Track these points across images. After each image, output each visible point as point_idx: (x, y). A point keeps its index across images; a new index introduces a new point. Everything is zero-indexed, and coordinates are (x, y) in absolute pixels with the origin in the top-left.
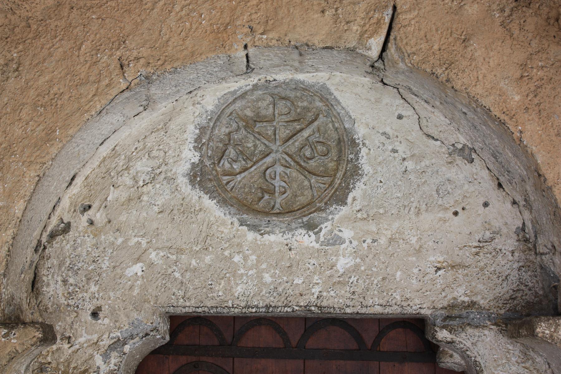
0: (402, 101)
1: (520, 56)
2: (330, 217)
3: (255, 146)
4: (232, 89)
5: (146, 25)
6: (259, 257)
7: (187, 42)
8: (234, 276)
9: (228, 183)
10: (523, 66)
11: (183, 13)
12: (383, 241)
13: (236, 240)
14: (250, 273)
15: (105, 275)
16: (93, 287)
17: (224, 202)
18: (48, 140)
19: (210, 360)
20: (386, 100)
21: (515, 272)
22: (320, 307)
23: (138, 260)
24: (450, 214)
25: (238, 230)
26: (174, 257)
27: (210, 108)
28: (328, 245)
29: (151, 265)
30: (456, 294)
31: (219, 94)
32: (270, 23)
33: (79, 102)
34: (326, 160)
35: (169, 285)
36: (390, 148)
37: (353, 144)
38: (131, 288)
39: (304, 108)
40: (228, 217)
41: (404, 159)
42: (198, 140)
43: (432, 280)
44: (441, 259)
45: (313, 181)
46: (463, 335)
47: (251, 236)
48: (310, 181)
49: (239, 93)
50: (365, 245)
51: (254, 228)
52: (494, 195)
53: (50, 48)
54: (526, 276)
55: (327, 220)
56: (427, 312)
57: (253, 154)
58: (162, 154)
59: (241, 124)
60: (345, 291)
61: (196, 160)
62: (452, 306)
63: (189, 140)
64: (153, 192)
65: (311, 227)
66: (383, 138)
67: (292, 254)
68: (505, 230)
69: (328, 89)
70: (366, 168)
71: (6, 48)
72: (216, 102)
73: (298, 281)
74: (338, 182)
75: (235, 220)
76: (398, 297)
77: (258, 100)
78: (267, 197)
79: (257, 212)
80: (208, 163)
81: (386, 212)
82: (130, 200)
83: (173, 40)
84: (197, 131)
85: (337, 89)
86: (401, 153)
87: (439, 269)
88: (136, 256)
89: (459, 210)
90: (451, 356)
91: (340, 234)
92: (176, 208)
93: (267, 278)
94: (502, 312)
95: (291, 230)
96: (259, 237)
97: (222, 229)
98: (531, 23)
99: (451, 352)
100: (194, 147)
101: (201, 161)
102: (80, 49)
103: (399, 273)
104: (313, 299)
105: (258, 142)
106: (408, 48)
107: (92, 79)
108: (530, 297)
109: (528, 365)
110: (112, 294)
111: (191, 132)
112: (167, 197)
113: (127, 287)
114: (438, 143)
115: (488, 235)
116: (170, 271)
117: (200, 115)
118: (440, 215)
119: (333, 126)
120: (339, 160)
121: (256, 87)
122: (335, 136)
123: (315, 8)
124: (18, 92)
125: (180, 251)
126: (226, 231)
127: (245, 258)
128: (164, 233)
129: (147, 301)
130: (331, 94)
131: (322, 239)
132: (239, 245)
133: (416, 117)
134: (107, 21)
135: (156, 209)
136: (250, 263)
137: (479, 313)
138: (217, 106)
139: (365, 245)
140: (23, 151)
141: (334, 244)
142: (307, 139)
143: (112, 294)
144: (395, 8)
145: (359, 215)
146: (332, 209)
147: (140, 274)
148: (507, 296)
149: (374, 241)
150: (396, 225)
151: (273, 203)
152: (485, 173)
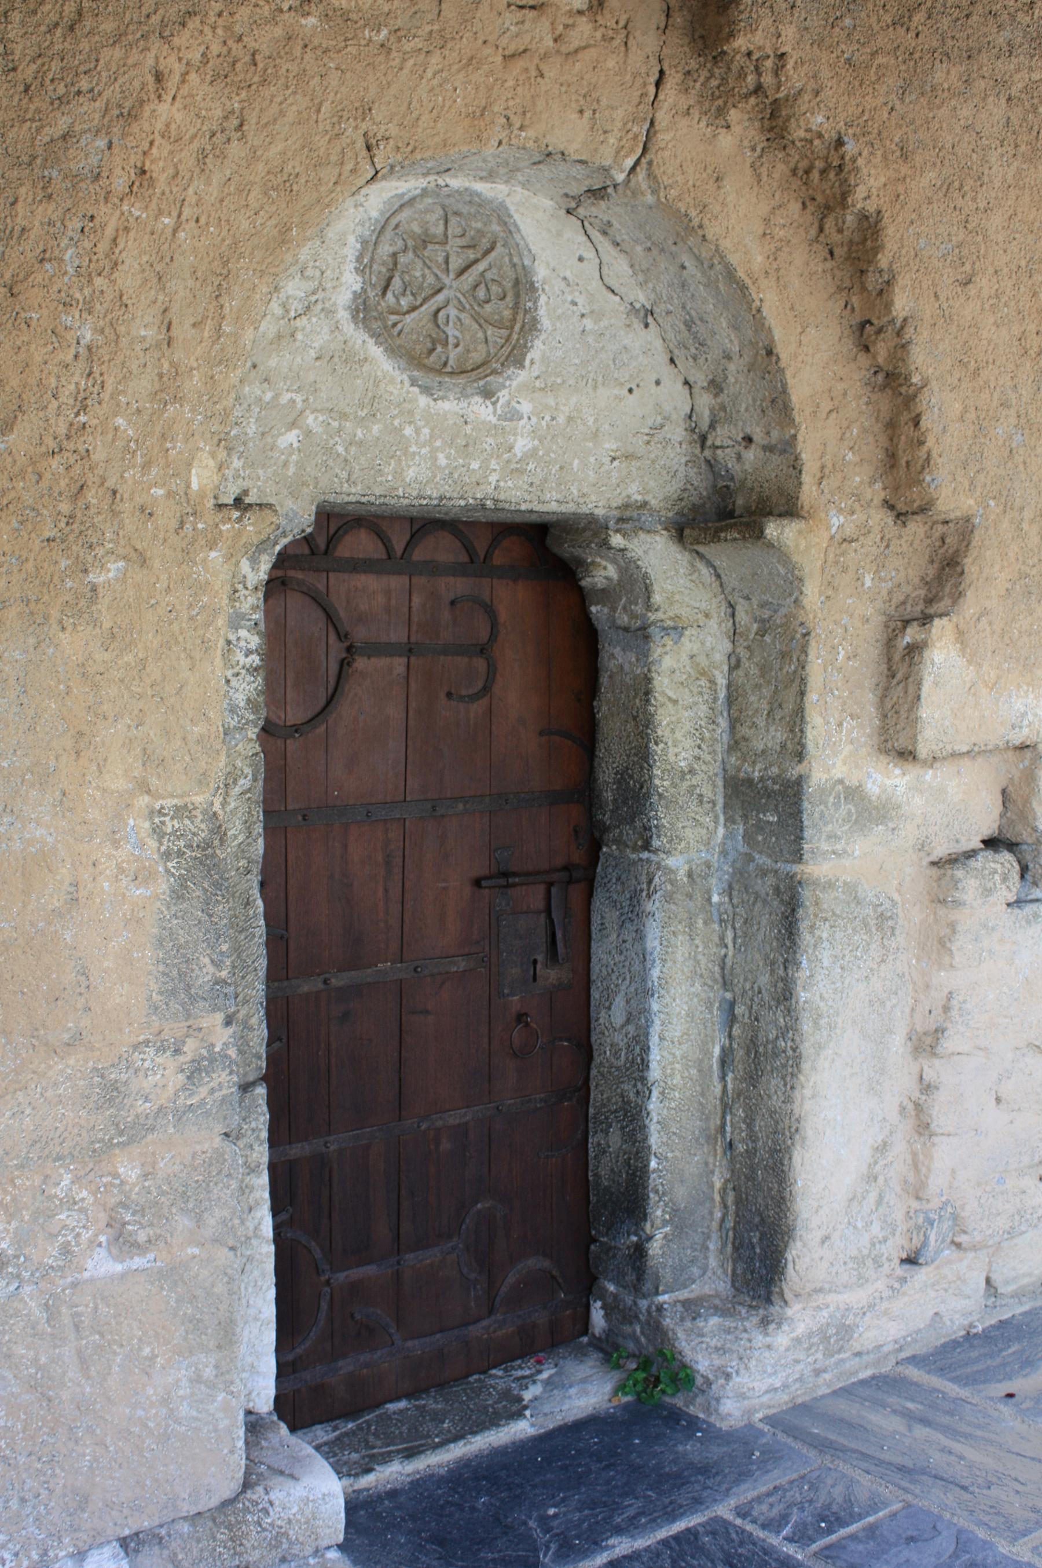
0: (585, 238)
1: (764, 209)
2: (508, 383)
3: (424, 276)
4: (400, 191)
5: (393, 90)
6: (432, 430)
7: (439, 125)
8: (405, 454)
9: (395, 325)
10: (767, 221)
11: (435, 82)
12: (561, 419)
13: (406, 405)
14: (423, 451)
15: (251, 444)
16: (236, 461)
17: (392, 351)
18: (283, 242)
19: (299, 575)
20: (568, 234)
21: (682, 468)
22: (496, 501)
23: (293, 425)
24: (625, 392)
25: (408, 392)
26: (335, 424)
27: (374, 214)
28: (505, 420)
29: (308, 433)
30: (630, 491)
31: (386, 195)
32: (528, 115)
33: (317, 191)
34: (502, 304)
35: (330, 463)
36: (569, 298)
37: (532, 288)
38: (285, 464)
39: (478, 231)
40: (397, 372)
41: (583, 316)
42: (359, 259)
43: (609, 472)
44: (614, 447)
45: (489, 333)
46: (636, 540)
47: (423, 401)
48: (485, 332)
49: (406, 198)
50: (544, 423)
51: (426, 390)
52: (666, 371)
53: (281, 103)
54: (692, 472)
55: (504, 387)
56: (600, 512)
57: (421, 288)
58: (318, 273)
59: (410, 243)
60: (522, 482)
61: (357, 287)
62: (626, 506)
63: (350, 258)
64: (309, 328)
65: (488, 394)
66: (563, 284)
67: (468, 429)
68: (674, 417)
69: (507, 209)
70: (546, 323)
71: (226, 91)
72: (381, 206)
73: (475, 465)
74: (515, 336)
75: (405, 377)
76: (575, 492)
77: (427, 211)
78: (439, 349)
79: (430, 369)
80: (371, 294)
81: (564, 382)
82: (279, 337)
83: (423, 118)
84: (359, 246)
85: (517, 211)
86: (580, 307)
87: (614, 459)
88: (290, 419)
89: (634, 387)
90: (605, 568)
91: (517, 406)
92: (337, 354)
93: (442, 461)
94: (670, 514)
95: (467, 397)
96: (432, 403)
97: (390, 388)
98: (781, 169)
99: (604, 563)
100: (356, 268)
101: (364, 290)
102: (318, 111)
103: (576, 462)
104: (490, 490)
105: (427, 271)
106: (665, 178)
107: (333, 158)
108: (695, 499)
109: (694, 577)
110: (261, 472)
111: (352, 248)
112: (326, 337)
113: (280, 463)
114: (617, 298)
115: (659, 420)
116: (332, 442)
117: (362, 223)
118: (616, 391)
119: (511, 260)
120: (516, 306)
121: (425, 192)
122: (511, 274)
123: (574, 105)
124: (244, 163)
125: (343, 416)
126: (396, 392)
127: (418, 431)
128: (323, 388)
129: (305, 484)
130: (510, 216)
131: (499, 412)
132: (411, 412)
133: (597, 261)
134: (348, 75)
135: (313, 353)
136: (422, 438)
137: (651, 515)
138: (382, 213)
139: (544, 423)
140: (252, 253)
141: (511, 420)
142: (482, 274)
143: (261, 472)
144: (652, 123)
145: (537, 384)
146: (510, 372)
147: (296, 445)
148: (675, 496)
149: (553, 419)
150: (574, 400)
151: (444, 359)
152: (658, 344)
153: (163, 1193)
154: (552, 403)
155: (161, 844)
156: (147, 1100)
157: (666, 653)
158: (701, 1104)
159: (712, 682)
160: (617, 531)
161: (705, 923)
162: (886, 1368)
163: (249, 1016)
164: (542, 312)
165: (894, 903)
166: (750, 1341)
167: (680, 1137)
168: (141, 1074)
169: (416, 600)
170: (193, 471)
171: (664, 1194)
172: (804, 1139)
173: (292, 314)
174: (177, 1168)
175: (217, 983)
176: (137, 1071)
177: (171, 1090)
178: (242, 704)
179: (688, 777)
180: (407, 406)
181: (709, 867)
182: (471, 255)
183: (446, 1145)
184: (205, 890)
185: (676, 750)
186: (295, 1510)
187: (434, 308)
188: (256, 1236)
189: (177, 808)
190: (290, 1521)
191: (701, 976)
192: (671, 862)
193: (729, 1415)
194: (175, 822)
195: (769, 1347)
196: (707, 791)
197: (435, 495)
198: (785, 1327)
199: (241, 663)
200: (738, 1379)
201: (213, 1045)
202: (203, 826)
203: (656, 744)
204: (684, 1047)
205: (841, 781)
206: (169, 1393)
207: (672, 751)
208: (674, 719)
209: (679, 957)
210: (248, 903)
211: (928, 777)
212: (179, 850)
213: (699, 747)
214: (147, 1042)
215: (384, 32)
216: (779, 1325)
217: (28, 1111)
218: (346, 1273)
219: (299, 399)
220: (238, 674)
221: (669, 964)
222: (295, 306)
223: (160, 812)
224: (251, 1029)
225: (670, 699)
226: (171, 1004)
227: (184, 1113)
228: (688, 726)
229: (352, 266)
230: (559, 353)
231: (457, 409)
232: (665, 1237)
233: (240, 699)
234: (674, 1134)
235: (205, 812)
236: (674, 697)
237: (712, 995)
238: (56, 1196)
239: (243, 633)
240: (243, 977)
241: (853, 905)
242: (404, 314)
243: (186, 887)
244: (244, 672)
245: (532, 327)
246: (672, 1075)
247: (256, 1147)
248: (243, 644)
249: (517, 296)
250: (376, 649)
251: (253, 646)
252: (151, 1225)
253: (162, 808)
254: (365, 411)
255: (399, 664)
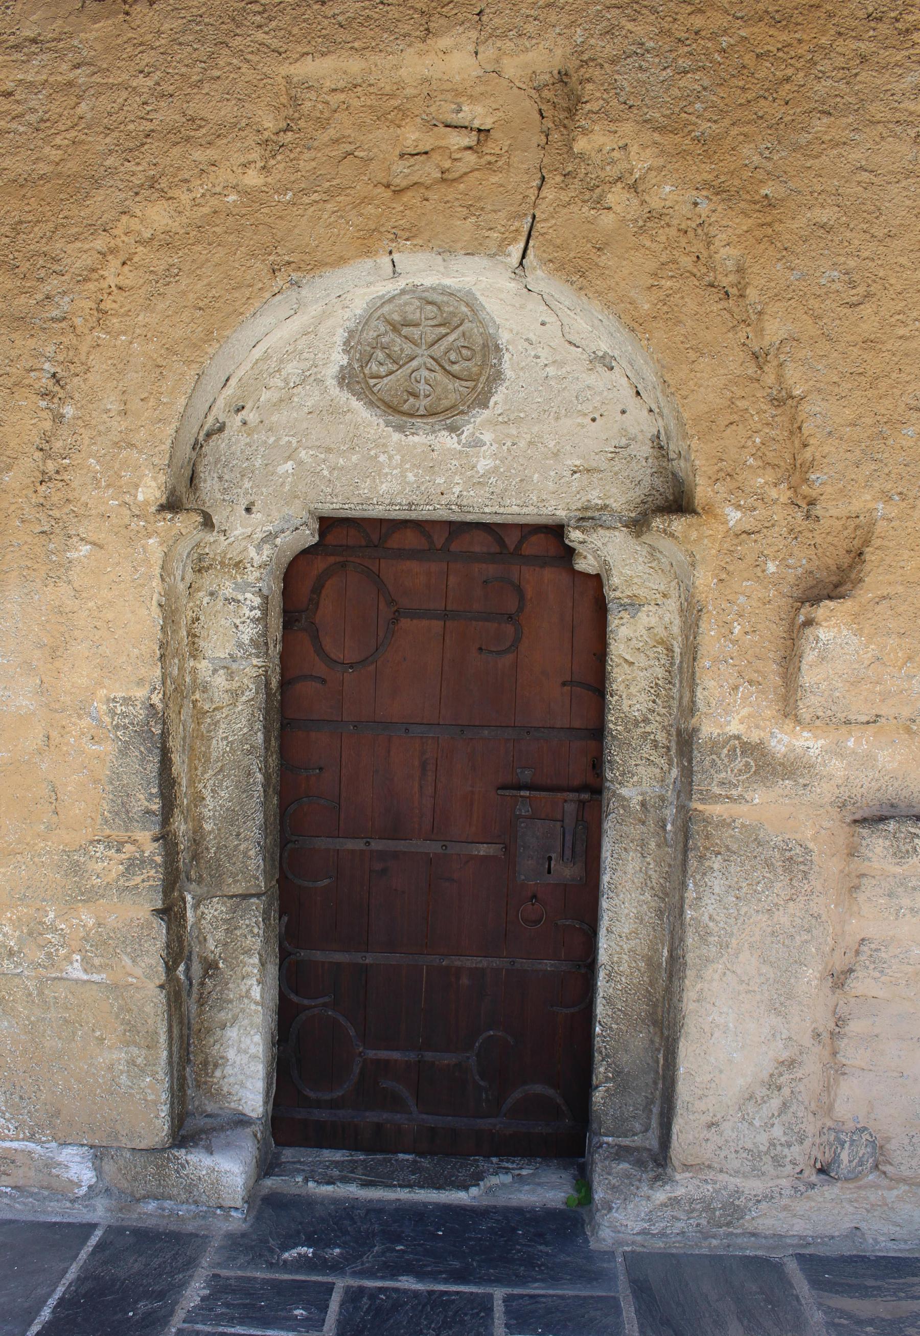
0: (546, 308)
2: (472, 420)
3: (402, 350)
4: (380, 294)
6: (403, 457)
8: (379, 475)
12: (522, 444)
14: (395, 472)
21: (648, 478)
23: (289, 458)
24: (588, 420)
26: (323, 456)
29: (301, 463)
36: (533, 354)
37: (497, 348)
38: (283, 484)
40: (375, 418)
46: (595, 535)
47: (396, 436)
49: (387, 297)
50: (505, 448)
51: (400, 428)
55: (470, 423)
60: (484, 492)
61: (345, 362)
63: (338, 343)
65: (453, 429)
68: (640, 437)
75: (381, 421)
77: (406, 304)
82: (281, 401)
84: (346, 334)
87: (575, 472)
88: (287, 454)
90: (585, 558)
91: (481, 436)
93: (411, 477)
95: (434, 432)
101: (349, 364)
110: (264, 490)
114: (580, 350)
125: (329, 450)
126: (372, 432)
127: (390, 458)
130: (476, 299)
131: (464, 441)
135: (306, 410)
136: (394, 462)
138: (365, 310)
143: (264, 490)
145: (500, 419)
146: (474, 412)
148: (639, 500)
149: (514, 444)
153: (111, 938)
154: (515, 432)
155: (113, 720)
156: (98, 877)
157: (622, 625)
158: (648, 992)
159: (670, 650)
160: (577, 528)
161: (658, 846)
162: (775, 1255)
163: (248, 850)
164: (506, 366)
165: (808, 851)
166: (638, 1188)
167: (625, 1014)
168: (94, 860)
169: (452, 580)
170: (140, 489)
171: (607, 1056)
172: (687, 1033)
173: (292, 385)
174: (120, 925)
175: (147, 813)
176: (91, 857)
177: (114, 874)
178: (247, 642)
179: (642, 725)
180: (383, 441)
181: (663, 801)
182: (443, 330)
183: (465, 981)
184: (141, 752)
185: (630, 702)
186: (204, 1172)
187: (409, 371)
188: (247, 997)
189: (124, 699)
190: (200, 1178)
191: (652, 888)
192: (624, 792)
193: (604, 1240)
194: (123, 708)
195: (648, 1198)
196: (661, 737)
197: (404, 502)
198: (667, 1187)
199: (247, 615)
200: (615, 1215)
201: (143, 852)
202: (141, 712)
203: (612, 696)
204: (633, 943)
205: (738, 737)
206: (112, 1065)
207: (626, 703)
208: (629, 677)
209: (629, 868)
210: (249, 774)
211: (851, 744)
212: (125, 725)
213: (654, 702)
214: (99, 841)
215: (290, 194)
216: (665, 1183)
217: (23, 868)
218: (374, 1052)
219: (294, 441)
220: (244, 622)
221: (619, 873)
222: (293, 380)
223: (113, 700)
224: (250, 858)
225: (626, 661)
226: (116, 820)
227: (124, 890)
228: (644, 684)
229: (340, 349)
230: (522, 395)
231: (425, 441)
232: (606, 1091)
233: (246, 639)
234: (619, 1010)
235: (143, 703)
236: (631, 660)
237: (662, 905)
238: (45, 923)
239: (249, 595)
240: (244, 823)
241: (754, 845)
242: (382, 377)
243: (129, 749)
244: (248, 621)
245: (497, 377)
246: (619, 963)
247: (249, 937)
248: (248, 602)
249: (485, 356)
250: (414, 614)
251: (256, 604)
252: (102, 956)
253: (115, 698)
254: (347, 446)
255: (437, 625)
